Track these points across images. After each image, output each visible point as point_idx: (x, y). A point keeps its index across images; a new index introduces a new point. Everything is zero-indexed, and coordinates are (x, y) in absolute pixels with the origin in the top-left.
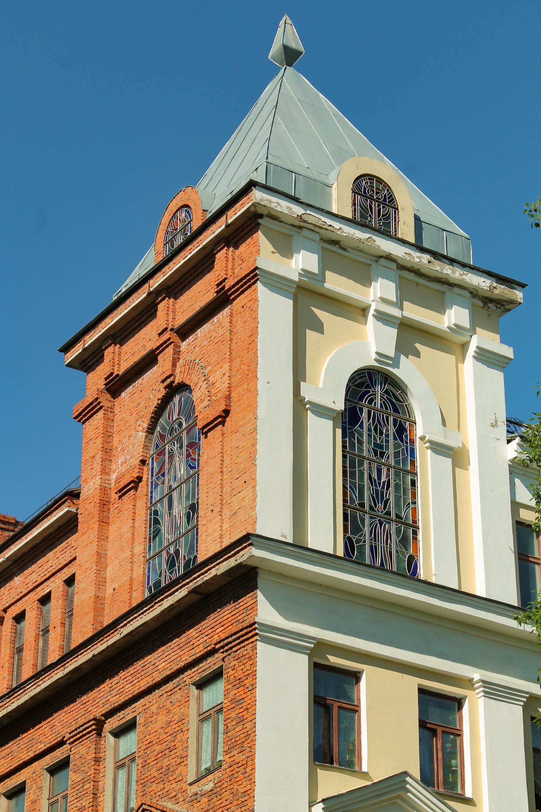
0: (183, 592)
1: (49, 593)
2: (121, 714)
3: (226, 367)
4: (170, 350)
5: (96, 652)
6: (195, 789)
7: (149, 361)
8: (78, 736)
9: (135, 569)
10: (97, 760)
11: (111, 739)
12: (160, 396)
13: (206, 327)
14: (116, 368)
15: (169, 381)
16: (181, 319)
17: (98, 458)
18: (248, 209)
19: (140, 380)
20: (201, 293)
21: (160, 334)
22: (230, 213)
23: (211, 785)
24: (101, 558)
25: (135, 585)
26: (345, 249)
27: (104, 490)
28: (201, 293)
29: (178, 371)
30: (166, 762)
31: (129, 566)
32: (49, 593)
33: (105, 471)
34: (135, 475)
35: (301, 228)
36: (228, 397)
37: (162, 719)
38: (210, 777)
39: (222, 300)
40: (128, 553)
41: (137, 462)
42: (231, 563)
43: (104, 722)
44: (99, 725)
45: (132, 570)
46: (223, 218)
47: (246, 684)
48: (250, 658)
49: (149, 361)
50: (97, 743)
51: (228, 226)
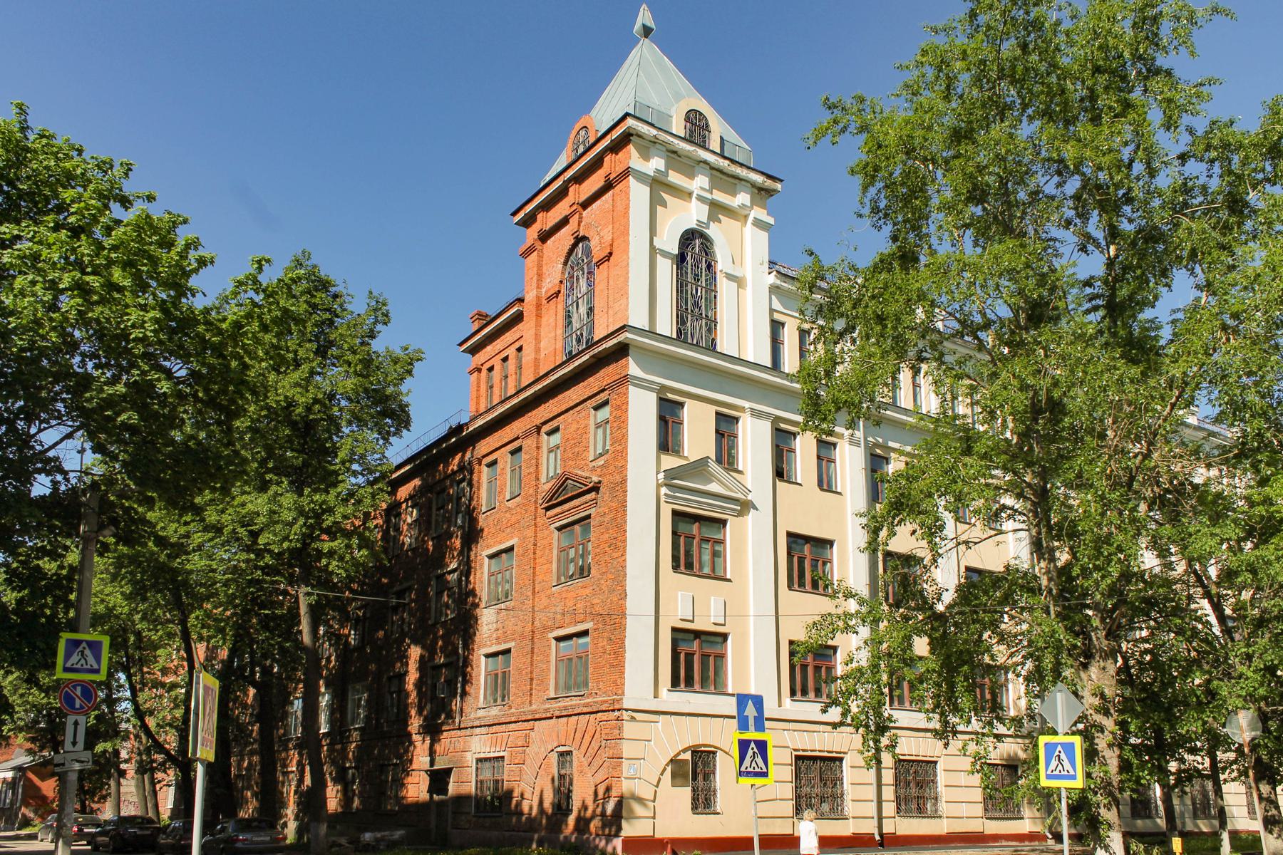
4: (577, 216)
7: (565, 222)
8: (527, 434)
10: (538, 448)
13: (598, 203)
16: (583, 198)
24: (537, 337)
27: (538, 298)
33: (539, 287)
37: (574, 426)
39: (608, 186)
42: (615, 341)
47: (622, 408)
49: (565, 222)
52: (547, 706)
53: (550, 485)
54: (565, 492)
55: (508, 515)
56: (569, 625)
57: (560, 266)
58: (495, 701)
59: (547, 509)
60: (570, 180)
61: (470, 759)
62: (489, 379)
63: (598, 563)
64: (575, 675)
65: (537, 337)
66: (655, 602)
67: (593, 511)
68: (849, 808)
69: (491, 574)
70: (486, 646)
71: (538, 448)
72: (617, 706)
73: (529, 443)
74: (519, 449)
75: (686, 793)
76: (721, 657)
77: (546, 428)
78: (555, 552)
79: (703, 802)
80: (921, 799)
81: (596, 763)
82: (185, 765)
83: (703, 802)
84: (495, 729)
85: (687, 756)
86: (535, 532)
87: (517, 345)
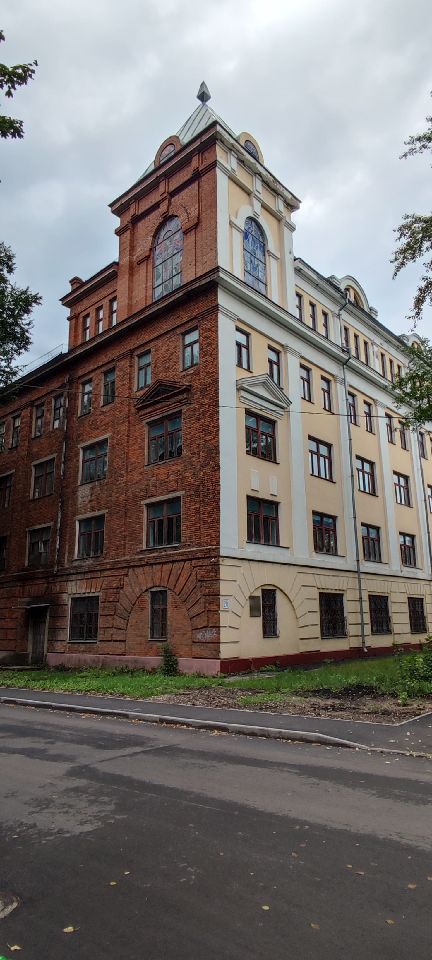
0: (181, 294)
1: (102, 305)
2: (107, 366)
3: (197, 206)
4: (166, 202)
5: (133, 322)
6: (183, 373)
7: (156, 206)
8: (121, 358)
9: (148, 292)
10: (131, 366)
11: (136, 358)
12: (160, 222)
13: (186, 191)
14: (137, 212)
15: (165, 215)
16: (172, 188)
17: (128, 249)
18: (213, 134)
19: (148, 217)
20: (185, 175)
21: (161, 195)
22: (203, 137)
23: (193, 371)
24: (131, 290)
25: (148, 298)
26: (244, 166)
27: (131, 262)
28: (185, 175)
29: (170, 210)
30: (167, 365)
31: (145, 291)
32: (102, 305)
33: (131, 255)
34: (147, 254)
35: (231, 150)
36: (198, 218)
37: (164, 348)
38: (193, 368)
39: (197, 176)
40: (144, 286)
41: (148, 249)
42: (208, 280)
43: (134, 352)
44: (132, 351)
45: (146, 292)
46: (199, 140)
47: (215, 329)
48: (215, 320)
49: (156, 206)
50: (131, 360)
51: (201, 143)
52: (141, 556)
53: (142, 393)
54: (161, 393)
55: (102, 417)
56: (161, 494)
57: (150, 239)
58: (88, 554)
59: (139, 409)
60: (161, 176)
61: (66, 599)
62: (85, 322)
63: (189, 446)
64: (167, 530)
65: (131, 290)
66: (237, 476)
67: (184, 409)
68: (396, 628)
69: (84, 462)
70: (81, 514)
71: (131, 366)
72: (213, 554)
73: (125, 363)
74: (113, 370)
75: (259, 621)
76: (276, 519)
77: (138, 352)
78: (146, 441)
79: (270, 629)
80: (334, 628)
81: (191, 601)
82: (351, 416)
83: (270, 629)
84: (89, 576)
85: (259, 593)
86: (129, 427)
87: (111, 297)
